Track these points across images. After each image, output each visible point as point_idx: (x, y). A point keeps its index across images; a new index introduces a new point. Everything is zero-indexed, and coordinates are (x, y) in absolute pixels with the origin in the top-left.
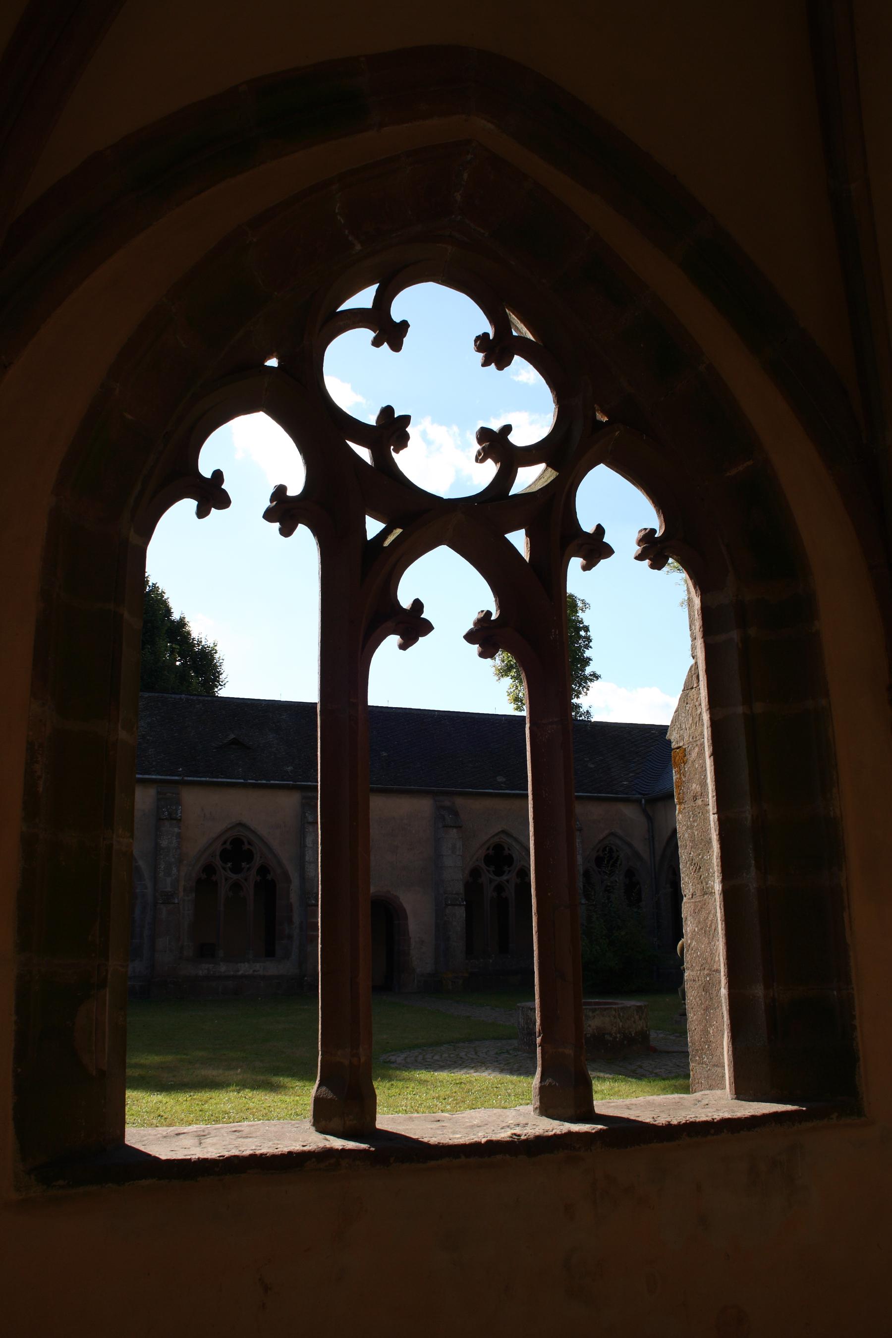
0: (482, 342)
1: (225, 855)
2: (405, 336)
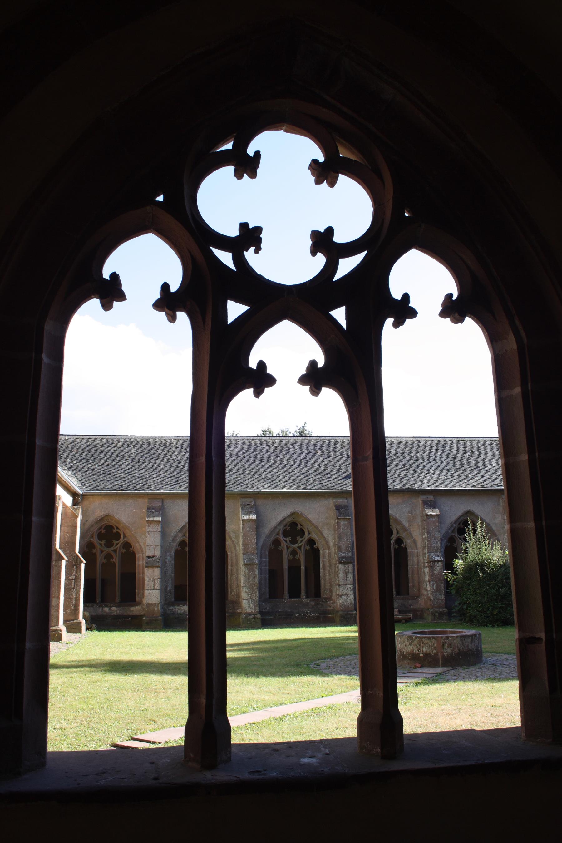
0: (315, 165)
1: (286, 533)
2: (258, 166)
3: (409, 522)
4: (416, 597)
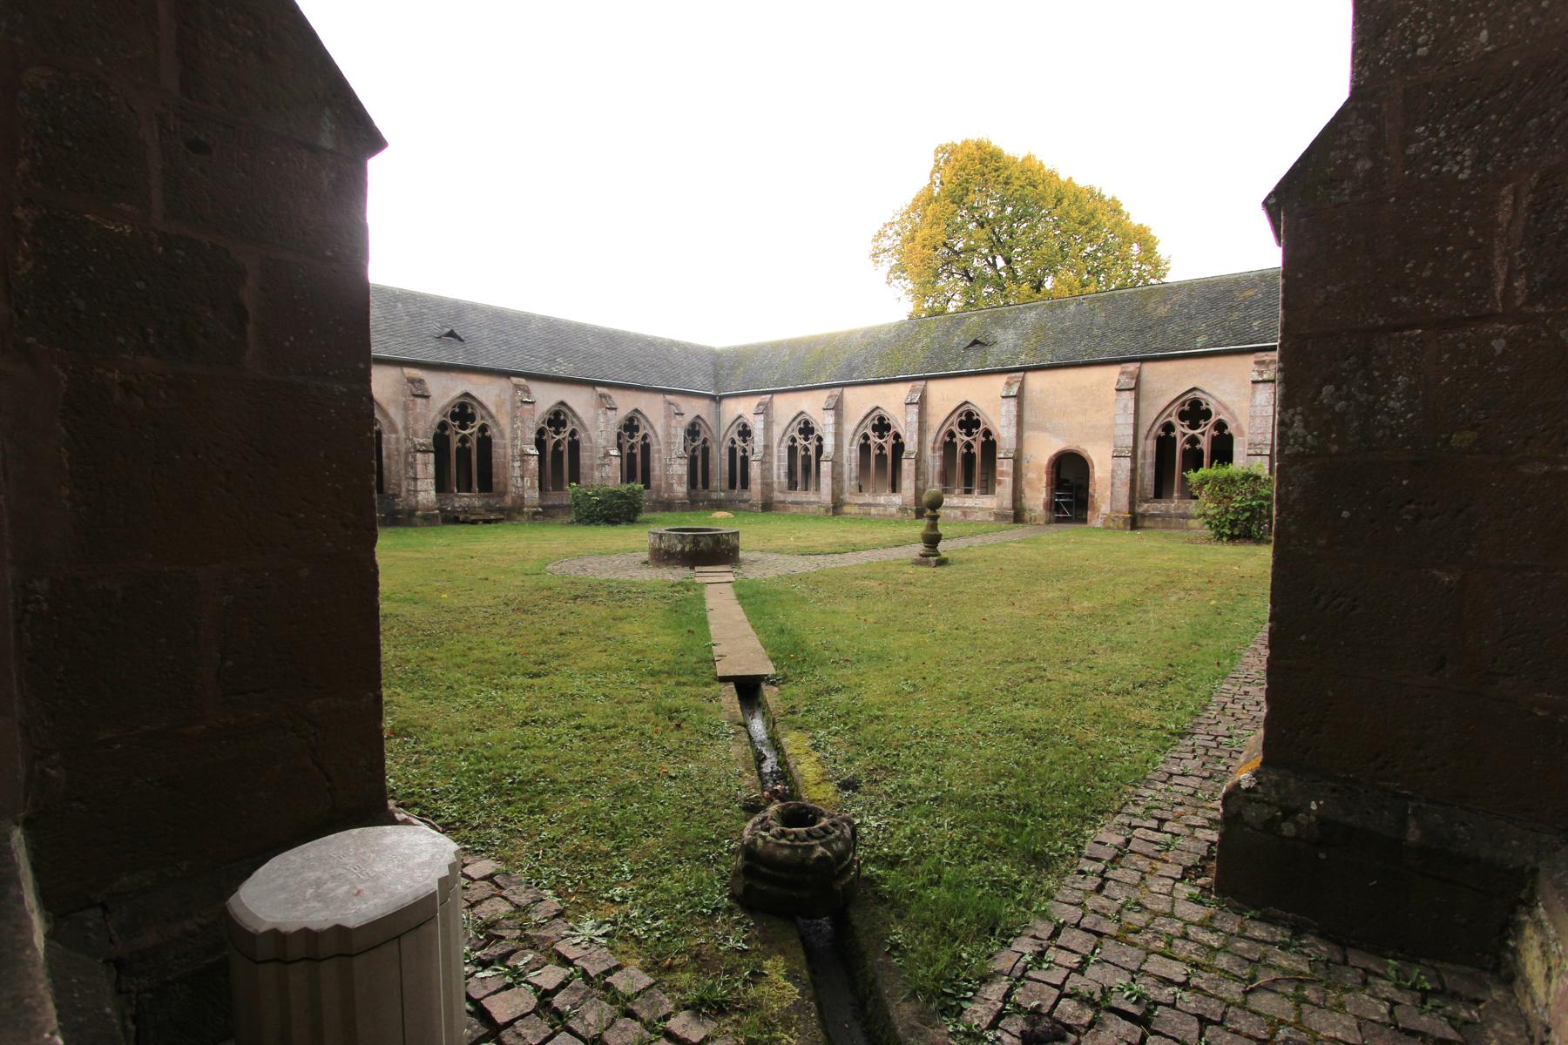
3: (497, 406)
4: (503, 494)
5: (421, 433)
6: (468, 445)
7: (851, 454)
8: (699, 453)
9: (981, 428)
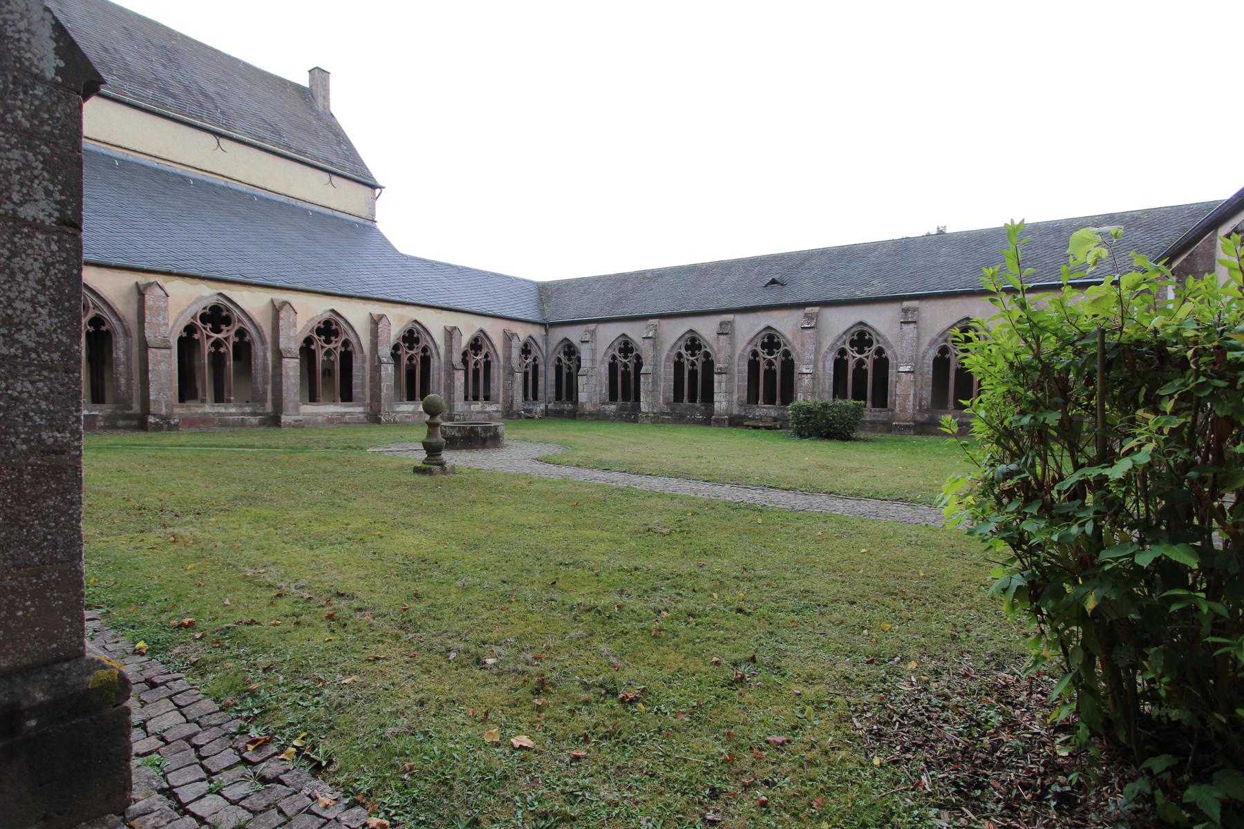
5: (722, 360)
6: (222, 350)
7: (666, 373)
8: (530, 370)
9: (702, 351)
